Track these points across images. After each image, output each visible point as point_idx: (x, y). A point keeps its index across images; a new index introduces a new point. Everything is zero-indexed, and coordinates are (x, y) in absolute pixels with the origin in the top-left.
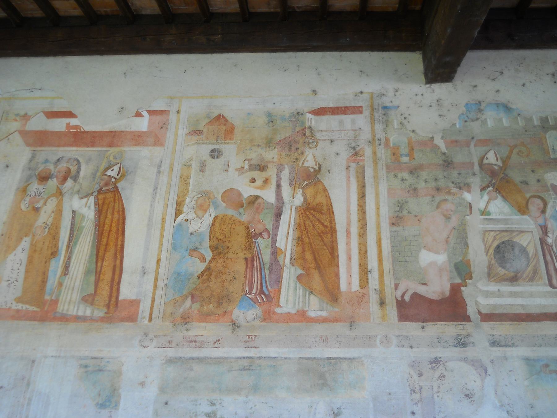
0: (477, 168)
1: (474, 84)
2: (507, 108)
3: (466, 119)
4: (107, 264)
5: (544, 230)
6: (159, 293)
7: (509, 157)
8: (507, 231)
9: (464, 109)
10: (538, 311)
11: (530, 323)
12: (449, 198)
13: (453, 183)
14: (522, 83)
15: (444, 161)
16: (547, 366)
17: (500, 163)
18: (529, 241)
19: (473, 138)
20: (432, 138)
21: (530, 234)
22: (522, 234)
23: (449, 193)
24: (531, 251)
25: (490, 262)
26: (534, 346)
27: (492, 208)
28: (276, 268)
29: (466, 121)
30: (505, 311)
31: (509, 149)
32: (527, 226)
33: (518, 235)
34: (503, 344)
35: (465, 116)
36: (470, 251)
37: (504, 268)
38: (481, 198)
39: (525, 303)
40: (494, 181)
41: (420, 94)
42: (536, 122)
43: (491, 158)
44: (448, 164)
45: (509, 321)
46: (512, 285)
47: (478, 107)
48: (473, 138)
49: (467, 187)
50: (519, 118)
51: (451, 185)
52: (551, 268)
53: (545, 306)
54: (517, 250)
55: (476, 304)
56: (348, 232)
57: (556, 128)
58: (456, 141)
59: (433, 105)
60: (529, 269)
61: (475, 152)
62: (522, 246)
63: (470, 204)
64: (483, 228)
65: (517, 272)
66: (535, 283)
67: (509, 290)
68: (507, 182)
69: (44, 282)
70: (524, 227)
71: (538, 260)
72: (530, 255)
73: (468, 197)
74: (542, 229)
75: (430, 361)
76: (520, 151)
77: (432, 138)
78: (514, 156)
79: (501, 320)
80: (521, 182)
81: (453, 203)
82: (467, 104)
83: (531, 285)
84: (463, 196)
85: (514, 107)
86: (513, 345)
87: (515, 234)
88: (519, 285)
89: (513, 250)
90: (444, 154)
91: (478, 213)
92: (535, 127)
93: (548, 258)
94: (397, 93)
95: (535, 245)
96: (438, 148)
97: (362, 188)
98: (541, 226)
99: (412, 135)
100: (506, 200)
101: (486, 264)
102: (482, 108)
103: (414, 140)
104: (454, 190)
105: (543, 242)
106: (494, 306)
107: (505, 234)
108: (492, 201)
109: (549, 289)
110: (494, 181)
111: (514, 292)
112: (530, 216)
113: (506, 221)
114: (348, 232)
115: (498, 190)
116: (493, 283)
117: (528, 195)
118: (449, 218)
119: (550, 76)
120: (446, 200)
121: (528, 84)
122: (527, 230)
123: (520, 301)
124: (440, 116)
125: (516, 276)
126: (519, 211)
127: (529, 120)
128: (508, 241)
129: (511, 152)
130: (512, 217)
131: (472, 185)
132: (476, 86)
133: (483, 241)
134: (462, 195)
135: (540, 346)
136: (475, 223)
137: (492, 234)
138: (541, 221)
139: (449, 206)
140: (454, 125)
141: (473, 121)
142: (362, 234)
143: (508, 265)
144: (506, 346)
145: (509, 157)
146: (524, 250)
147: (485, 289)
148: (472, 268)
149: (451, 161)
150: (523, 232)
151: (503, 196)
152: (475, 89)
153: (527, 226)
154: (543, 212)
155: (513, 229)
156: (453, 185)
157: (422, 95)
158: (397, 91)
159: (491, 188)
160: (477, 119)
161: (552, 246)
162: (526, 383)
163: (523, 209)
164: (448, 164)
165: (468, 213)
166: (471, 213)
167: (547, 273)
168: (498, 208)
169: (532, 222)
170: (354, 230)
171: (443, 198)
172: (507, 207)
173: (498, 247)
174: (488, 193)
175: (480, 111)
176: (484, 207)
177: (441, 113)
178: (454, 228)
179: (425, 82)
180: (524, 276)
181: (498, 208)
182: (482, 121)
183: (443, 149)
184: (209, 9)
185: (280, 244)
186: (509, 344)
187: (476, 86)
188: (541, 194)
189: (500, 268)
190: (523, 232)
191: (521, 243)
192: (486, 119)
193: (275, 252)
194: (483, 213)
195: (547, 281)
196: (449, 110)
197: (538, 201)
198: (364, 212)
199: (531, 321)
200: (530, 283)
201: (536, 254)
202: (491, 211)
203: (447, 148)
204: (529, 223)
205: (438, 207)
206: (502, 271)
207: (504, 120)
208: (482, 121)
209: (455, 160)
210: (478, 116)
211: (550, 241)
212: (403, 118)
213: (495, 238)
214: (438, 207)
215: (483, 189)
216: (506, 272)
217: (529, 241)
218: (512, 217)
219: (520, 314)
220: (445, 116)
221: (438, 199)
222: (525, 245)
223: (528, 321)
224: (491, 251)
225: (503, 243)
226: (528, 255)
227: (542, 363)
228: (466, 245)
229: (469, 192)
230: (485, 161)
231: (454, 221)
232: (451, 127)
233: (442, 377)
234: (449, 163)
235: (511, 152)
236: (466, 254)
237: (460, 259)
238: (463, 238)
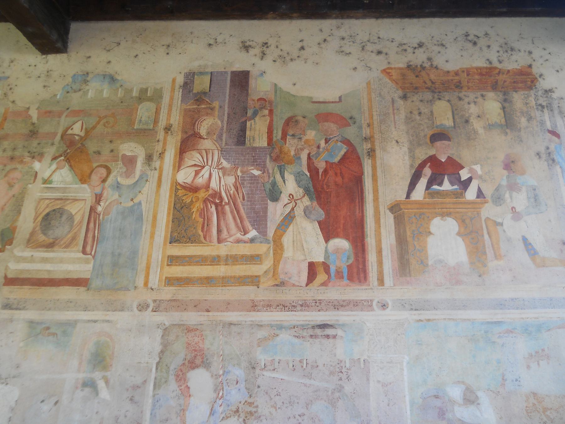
0: (58, 137)
1: (88, 55)
2: (112, 79)
3: (70, 90)
5: (98, 198)
7: (94, 128)
8: (61, 199)
9: (71, 80)
10: (62, 276)
11: (49, 288)
12: (19, 166)
13: (29, 152)
14: (135, 54)
15: (31, 131)
16: (48, 328)
17: (82, 134)
18: (78, 210)
19: (68, 109)
20: (29, 108)
21: (84, 202)
22: (76, 202)
23: (21, 162)
24: (77, 219)
25: (34, 228)
26: (43, 310)
27: (56, 178)
29: (68, 92)
30: (30, 276)
31: (98, 119)
32: (83, 195)
33: (71, 203)
34: (14, 307)
35: (69, 87)
36: (21, 218)
37: (45, 234)
38: (49, 167)
39: (52, 269)
40: (69, 151)
41: (34, 64)
42: (135, 94)
43: (77, 129)
44: (33, 133)
45: (30, 285)
46: (46, 251)
47: (84, 78)
48: (68, 109)
50: (120, 89)
51: (27, 154)
52: (90, 235)
53: (70, 272)
54: (64, 217)
55: (6, 269)
58: (50, 112)
59: (42, 75)
60: (70, 235)
61: (64, 122)
62: (71, 214)
63: (37, 172)
64: (41, 196)
65: (56, 239)
66: (69, 249)
67: (42, 256)
68: (81, 152)
70: (80, 195)
71: (81, 227)
72: (75, 223)
73: (37, 166)
74: (96, 198)
76: (107, 122)
77: (29, 108)
78: (100, 127)
79: (22, 285)
80: (95, 152)
81: (21, 172)
82: (75, 75)
83: (65, 252)
84: (33, 166)
85: (119, 78)
86: (24, 308)
87: (68, 202)
88: (53, 251)
89: (61, 217)
90: (33, 124)
91: (41, 181)
92: (132, 98)
93: (92, 225)
94: (12, 64)
95: (84, 213)
96: (30, 117)
98: (96, 195)
99: (11, 105)
100: (72, 169)
101: (30, 230)
102: (88, 79)
103: (11, 110)
104: (28, 159)
105: (92, 209)
106: (22, 271)
107: (59, 202)
108: (58, 171)
109: (81, 255)
110: (69, 151)
111: (47, 258)
112: (89, 185)
113: (64, 190)
115: (68, 160)
116: (29, 249)
117: (95, 165)
118: (13, 186)
119: (165, 47)
120: (15, 169)
121: (140, 56)
122: (81, 198)
123: (48, 267)
124: (45, 86)
125: (54, 242)
126: (81, 180)
127: (129, 91)
128: (60, 208)
129: (98, 123)
130: (71, 186)
131: (46, 155)
132: (89, 57)
133: (36, 209)
134: (32, 164)
135: (50, 309)
136: (36, 191)
137: (47, 202)
138: (98, 190)
139: (16, 175)
140: (55, 95)
141: (75, 92)
143: (50, 232)
144: (17, 309)
145: (94, 128)
146: (71, 218)
147: (20, 254)
148: (16, 235)
149: (37, 131)
150: (77, 200)
151: (71, 166)
152: (88, 59)
153: (83, 195)
154: (104, 181)
155: (77, 198)
156: (28, 154)
157: (35, 66)
158: (12, 62)
159: (62, 158)
160: (80, 90)
161: (99, 215)
162: (21, 344)
163: (84, 179)
164: (33, 133)
165: (32, 181)
166: (34, 182)
167: (85, 240)
168: (62, 177)
169: (89, 190)
171: (13, 166)
172: (70, 176)
173: (48, 215)
174: (57, 163)
175: (86, 82)
176: (48, 175)
177: (46, 84)
178: (14, 196)
180: (62, 242)
181: (62, 177)
182: (84, 92)
183: (35, 120)
184: (437, 215)
186: (21, 307)
187: (89, 57)
188: (109, 164)
189: (41, 235)
190: (77, 200)
191: (71, 211)
192: (88, 90)
194: (45, 182)
195: (81, 248)
196: (55, 81)
197: (103, 171)
199: (51, 286)
200: (65, 250)
201: (81, 222)
202: (53, 180)
203: (38, 119)
205: (5, 176)
206: (42, 238)
207: (105, 92)
208: (84, 92)
209: (41, 131)
210: (82, 87)
211: (99, 209)
212: (8, 89)
213: (47, 206)
214: (5, 176)
215: (54, 158)
216: (46, 239)
217: (78, 210)
218: (71, 186)
219: (44, 279)
220: (49, 87)
221: (8, 168)
222: (73, 213)
223: (48, 286)
224: (40, 219)
225: (54, 210)
226: (73, 222)
227: (44, 326)
228: (19, 212)
229: (40, 161)
230: (70, 132)
231: (16, 189)
232: (51, 98)
234: (34, 133)
235: (98, 123)
236: (16, 221)
237: (9, 225)
238: (19, 205)
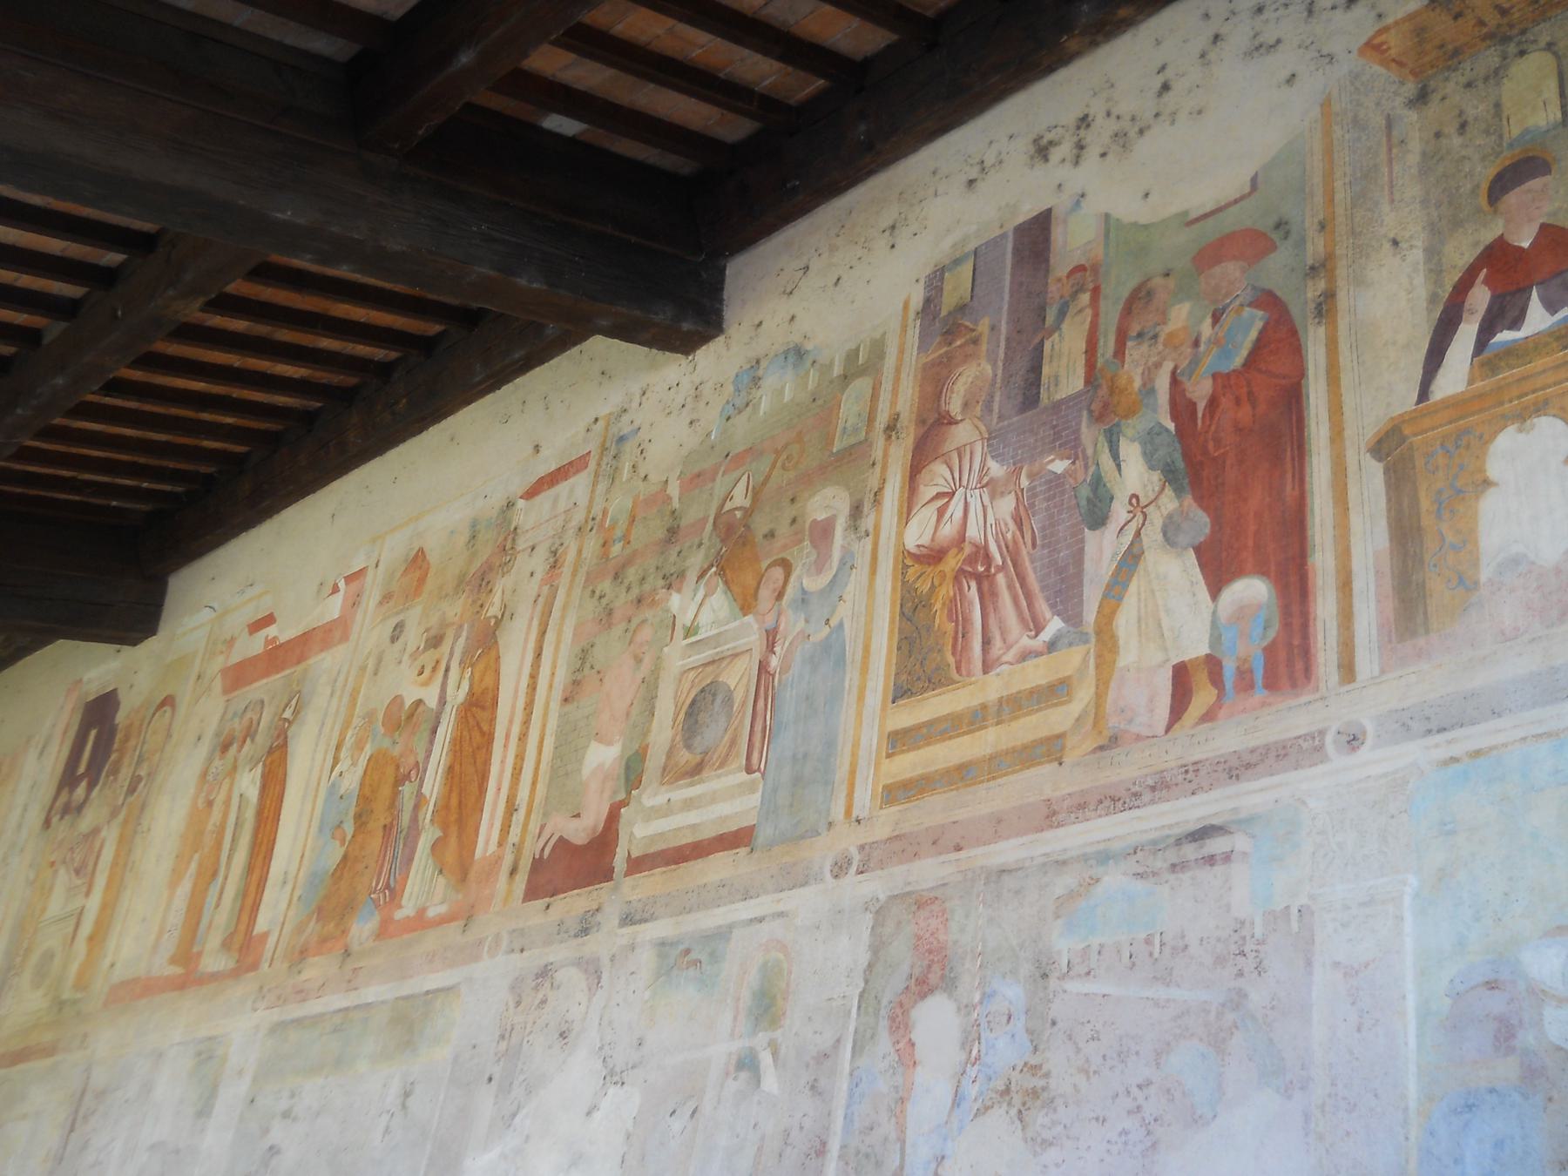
4: (256, 876)
6: (291, 913)
16: (687, 952)
24: (738, 698)
28: (415, 829)
34: (638, 917)
49: (673, 581)
56: (507, 736)
57: (1561, 1001)
69: (198, 924)
75: (1331, 62)
97: (543, 633)
114: (507, 736)
142: (523, 737)
151: (726, 583)
170: (516, 730)
179: (1197, 542)
185: (426, 790)
193: (420, 800)
198: (534, 689)
204: (749, 632)
233: (544, 1002)
